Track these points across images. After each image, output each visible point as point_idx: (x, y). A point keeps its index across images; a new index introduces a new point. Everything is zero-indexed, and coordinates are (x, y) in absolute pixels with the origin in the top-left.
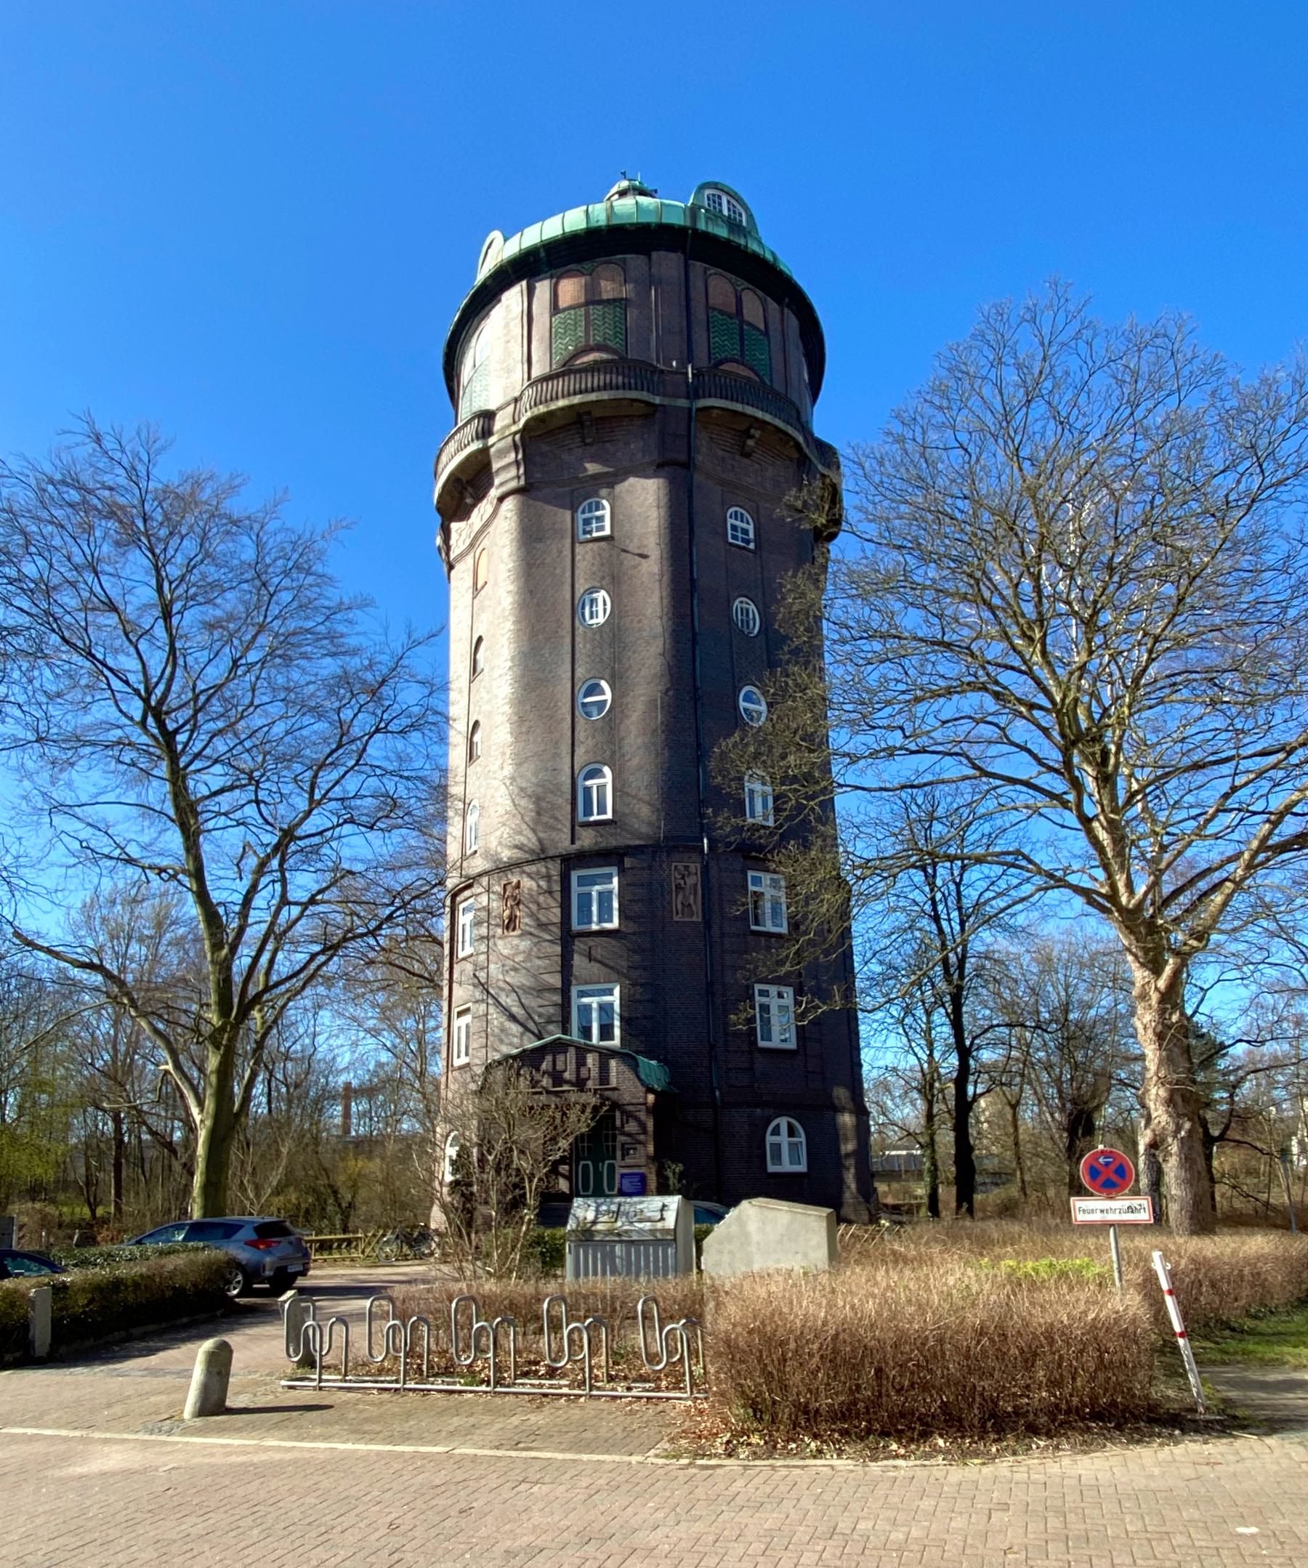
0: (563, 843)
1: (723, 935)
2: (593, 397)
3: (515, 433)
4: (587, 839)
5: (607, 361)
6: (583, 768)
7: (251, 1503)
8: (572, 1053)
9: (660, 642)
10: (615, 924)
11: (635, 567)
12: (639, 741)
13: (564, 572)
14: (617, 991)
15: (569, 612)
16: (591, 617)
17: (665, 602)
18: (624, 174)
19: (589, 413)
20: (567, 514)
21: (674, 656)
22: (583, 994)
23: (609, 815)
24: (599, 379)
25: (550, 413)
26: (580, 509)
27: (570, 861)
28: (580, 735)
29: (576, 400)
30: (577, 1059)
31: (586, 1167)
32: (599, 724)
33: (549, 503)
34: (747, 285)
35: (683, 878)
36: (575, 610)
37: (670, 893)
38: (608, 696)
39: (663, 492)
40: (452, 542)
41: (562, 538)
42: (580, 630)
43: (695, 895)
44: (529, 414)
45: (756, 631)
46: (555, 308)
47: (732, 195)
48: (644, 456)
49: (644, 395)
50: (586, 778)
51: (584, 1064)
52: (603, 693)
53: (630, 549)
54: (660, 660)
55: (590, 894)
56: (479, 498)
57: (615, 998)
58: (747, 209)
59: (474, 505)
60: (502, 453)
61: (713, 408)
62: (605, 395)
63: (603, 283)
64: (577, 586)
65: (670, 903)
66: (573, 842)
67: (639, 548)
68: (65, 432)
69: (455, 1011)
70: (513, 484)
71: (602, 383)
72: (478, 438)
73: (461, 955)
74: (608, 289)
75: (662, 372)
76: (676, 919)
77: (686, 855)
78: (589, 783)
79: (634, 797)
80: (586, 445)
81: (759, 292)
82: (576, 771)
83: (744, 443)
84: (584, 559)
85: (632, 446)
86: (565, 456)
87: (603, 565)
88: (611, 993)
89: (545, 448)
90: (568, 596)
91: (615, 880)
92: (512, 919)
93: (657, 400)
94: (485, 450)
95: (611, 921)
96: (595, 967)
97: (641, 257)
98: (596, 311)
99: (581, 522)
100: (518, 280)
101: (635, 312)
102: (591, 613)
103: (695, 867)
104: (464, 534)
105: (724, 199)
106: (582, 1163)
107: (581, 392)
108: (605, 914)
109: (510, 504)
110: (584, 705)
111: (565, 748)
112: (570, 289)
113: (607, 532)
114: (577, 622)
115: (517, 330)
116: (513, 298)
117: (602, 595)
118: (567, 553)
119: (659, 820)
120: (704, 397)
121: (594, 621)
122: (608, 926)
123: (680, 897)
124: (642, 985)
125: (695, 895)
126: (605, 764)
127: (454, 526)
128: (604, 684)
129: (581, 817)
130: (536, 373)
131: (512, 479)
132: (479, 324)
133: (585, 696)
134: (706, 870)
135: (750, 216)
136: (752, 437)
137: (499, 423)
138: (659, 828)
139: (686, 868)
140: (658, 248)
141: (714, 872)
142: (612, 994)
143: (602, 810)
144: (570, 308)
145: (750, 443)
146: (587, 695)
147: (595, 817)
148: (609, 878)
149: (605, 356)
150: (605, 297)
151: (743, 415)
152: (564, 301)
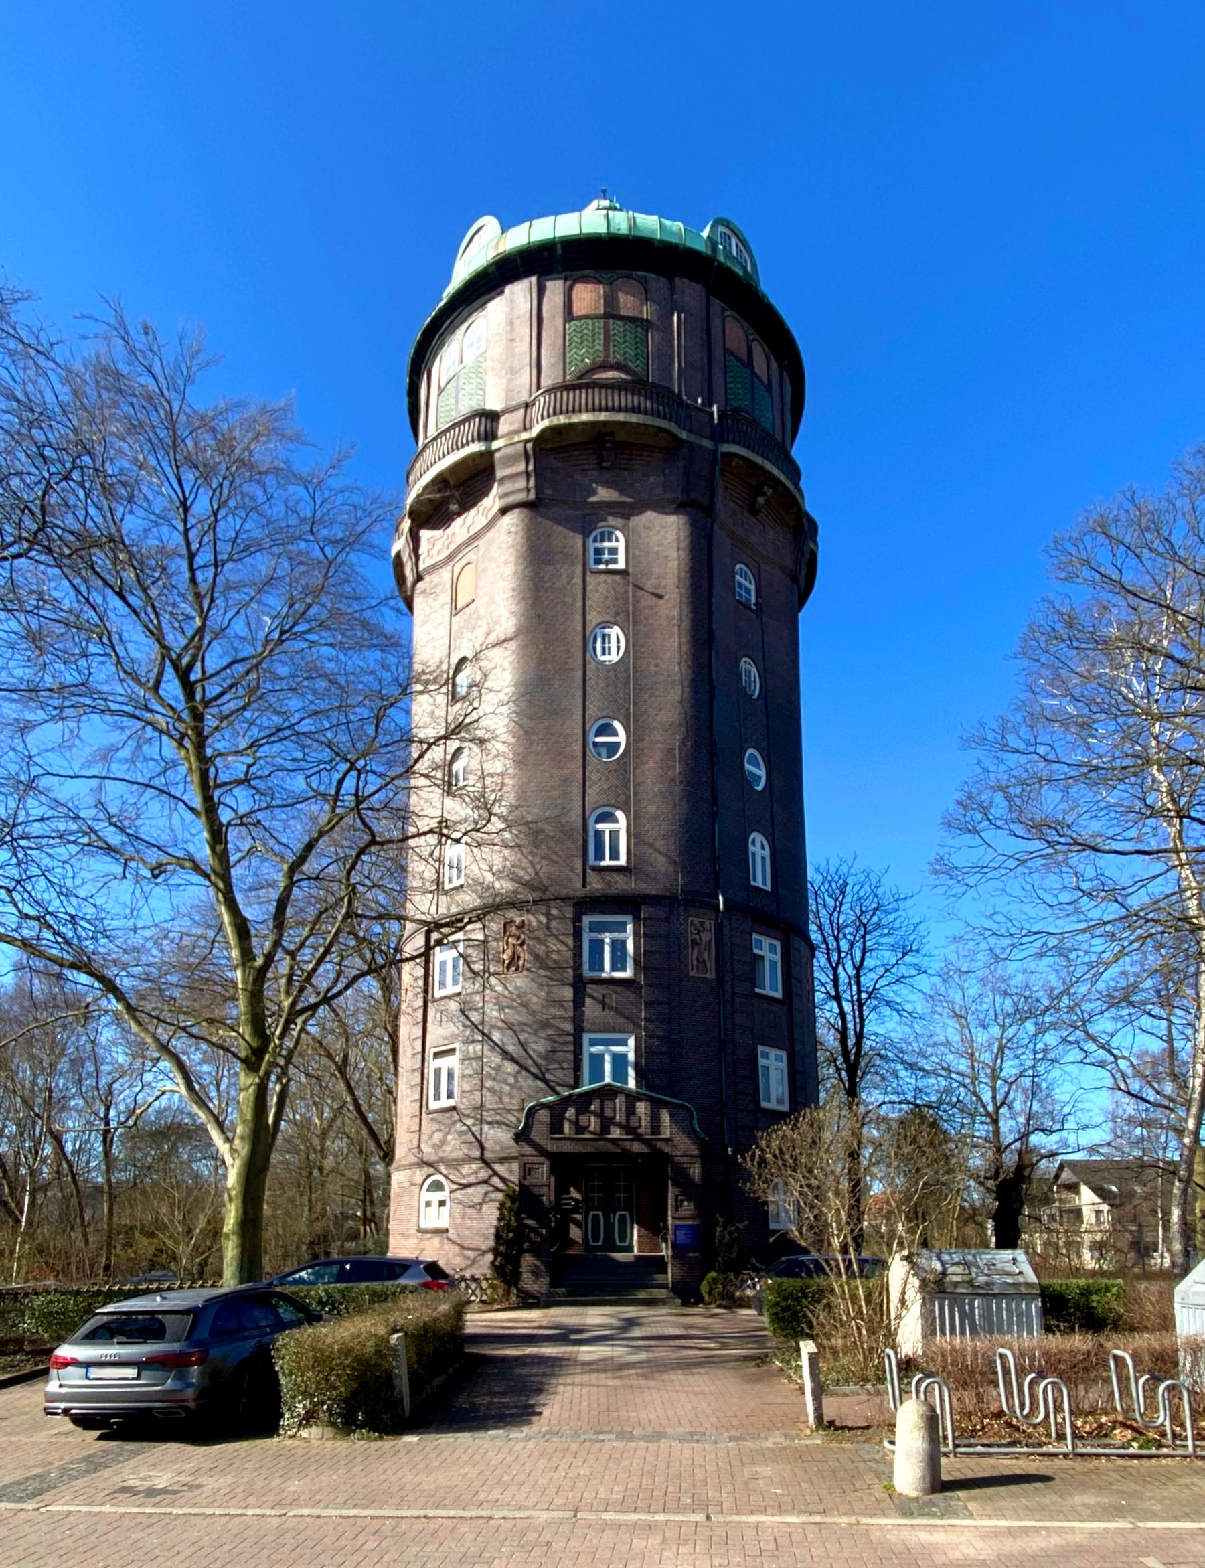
0: (576, 888)
1: (734, 994)
2: (620, 417)
3: (527, 441)
4: (596, 884)
5: (624, 381)
6: (594, 810)
7: (35, 1557)
8: (620, 1101)
9: (679, 690)
10: (628, 974)
11: (652, 608)
12: (656, 789)
13: (575, 601)
14: (631, 1042)
15: (580, 644)
16: (604, 654)
17: (684, 648)
18: (604, 192)
19: (611, 434)
20: (579, 539)
21: (693, 706)
22: (593, 1043)
23: (622, 861)
24: (626, 400)
25: (571, 426)
26: (591, 538)
27: (585, 905)
28: (593, 776)
29: (603, 416)
30: (627, 1107)
31: (596, 1218)
32: (612, 767)
33: (560, 524)
34: (758, 337)
35: (698, 933)
36: (586, 644)
37: (686, 947)
38: (622, 738)
39: (684, 533)
40: (422, 550)
41: (573, 564)
42: (591, 667)
43: (709, 951)
44: (546, 423)
45: (757, 693)
46: (569, 315)
47: (742, 241)
48: (665, 491)
49: (672, 427)
50: (597, 821)
51: (634, 1113)
52: (615, 734)
53: (646, 587)
54: (680, 709)
55: (602, 942)
56: (466, 506)
57: (629, 1049)
58: (752, 257)
59: (459, 514)
60: (510, 460)
61: (737, 455)
62: (634, 418)
63: (620, 294)
64: (588, 618)
65: (686, 957)
66: (584, 886)
67: (656, 587)
68: (83, 317)
69: (430, 1053)
70: (521, 497)
71: (629, 404)
72: (479, 439)
73: (438, 993)
74: (628, 303)
75: (688, 406)
76: (692, 974)
77: (702, 911)
78: (600, 826)
79: (651, 846)
80: (602, 468)
81: (766, 348)
82: (587, 813)
83: (755, 501)
84: (597, 591)
85: (652, 479)
86: (578, 477)
87: (617, 599)
88: (624, 1043)
89: (556, 464)
90: (579, 628)
91: (630, 927)
92: (515, 958)
93: (684, 435)
94: (489, 454)
95: (624, 969)
96: (609, 1016)
97: (663, 280)
98: (616, 327)
99: (592, 552)
100: (527, 274)
101: (658, 336)
102: (604, 649)
103: (709, 924)
104: (439, 545)
105: (734, 241)
106: (592, 1213)
107: (607, 410)
108: (618, 964)
109: (510, 519)
110: (595, 744)
111: (576, 789)
112: (587, 296)
113: (621, 565)
114: (588, 656)
115: (524, 331)
116: (519, 293)
117: (615, 632)
118: (578, 580)
119: (676, 872)
120: (728, 442)
121: (606, 658)
122: (618, 975)
123: (695, 952)
124: (658, 1038)
125: (709, 951)
126: (618, 808)
127: (425, 534)
128: (617, 725)
129: (592, 861)
130: (546, 382)
131: (520, 491)
132: (470, 314)
133: (597, 735)
134: (719, 928)
135: (754, 266)
136: (764, 494)
137: (504, 426)
138: (676, 880)
139: (702, 923)
140: (682, 275)
141: (726, 930)
142: (626, 1045)
143: (615, 855)
144: (587, 317)
145: (761, 500)
146: (597, 735)
147: (607, 862)
148: (621, 927)
149: (623, 376)
150: (623, 312)
151: (761, 468)
152: (579, 309)
